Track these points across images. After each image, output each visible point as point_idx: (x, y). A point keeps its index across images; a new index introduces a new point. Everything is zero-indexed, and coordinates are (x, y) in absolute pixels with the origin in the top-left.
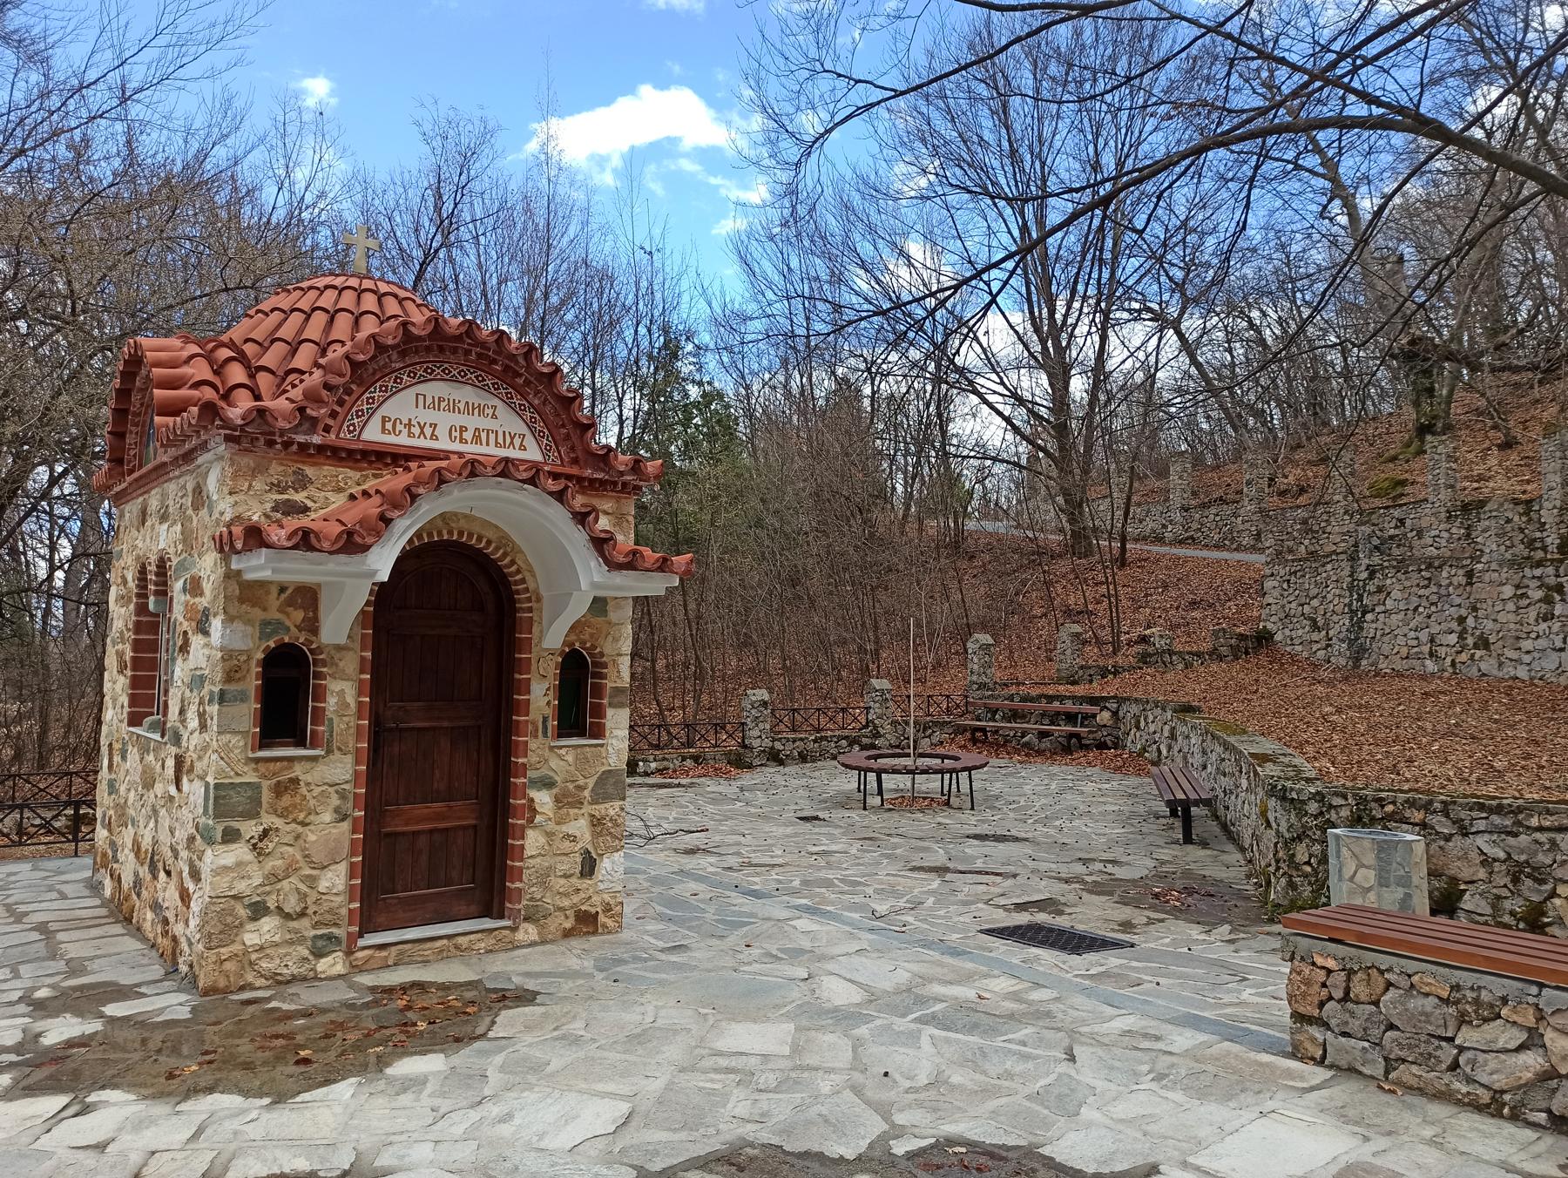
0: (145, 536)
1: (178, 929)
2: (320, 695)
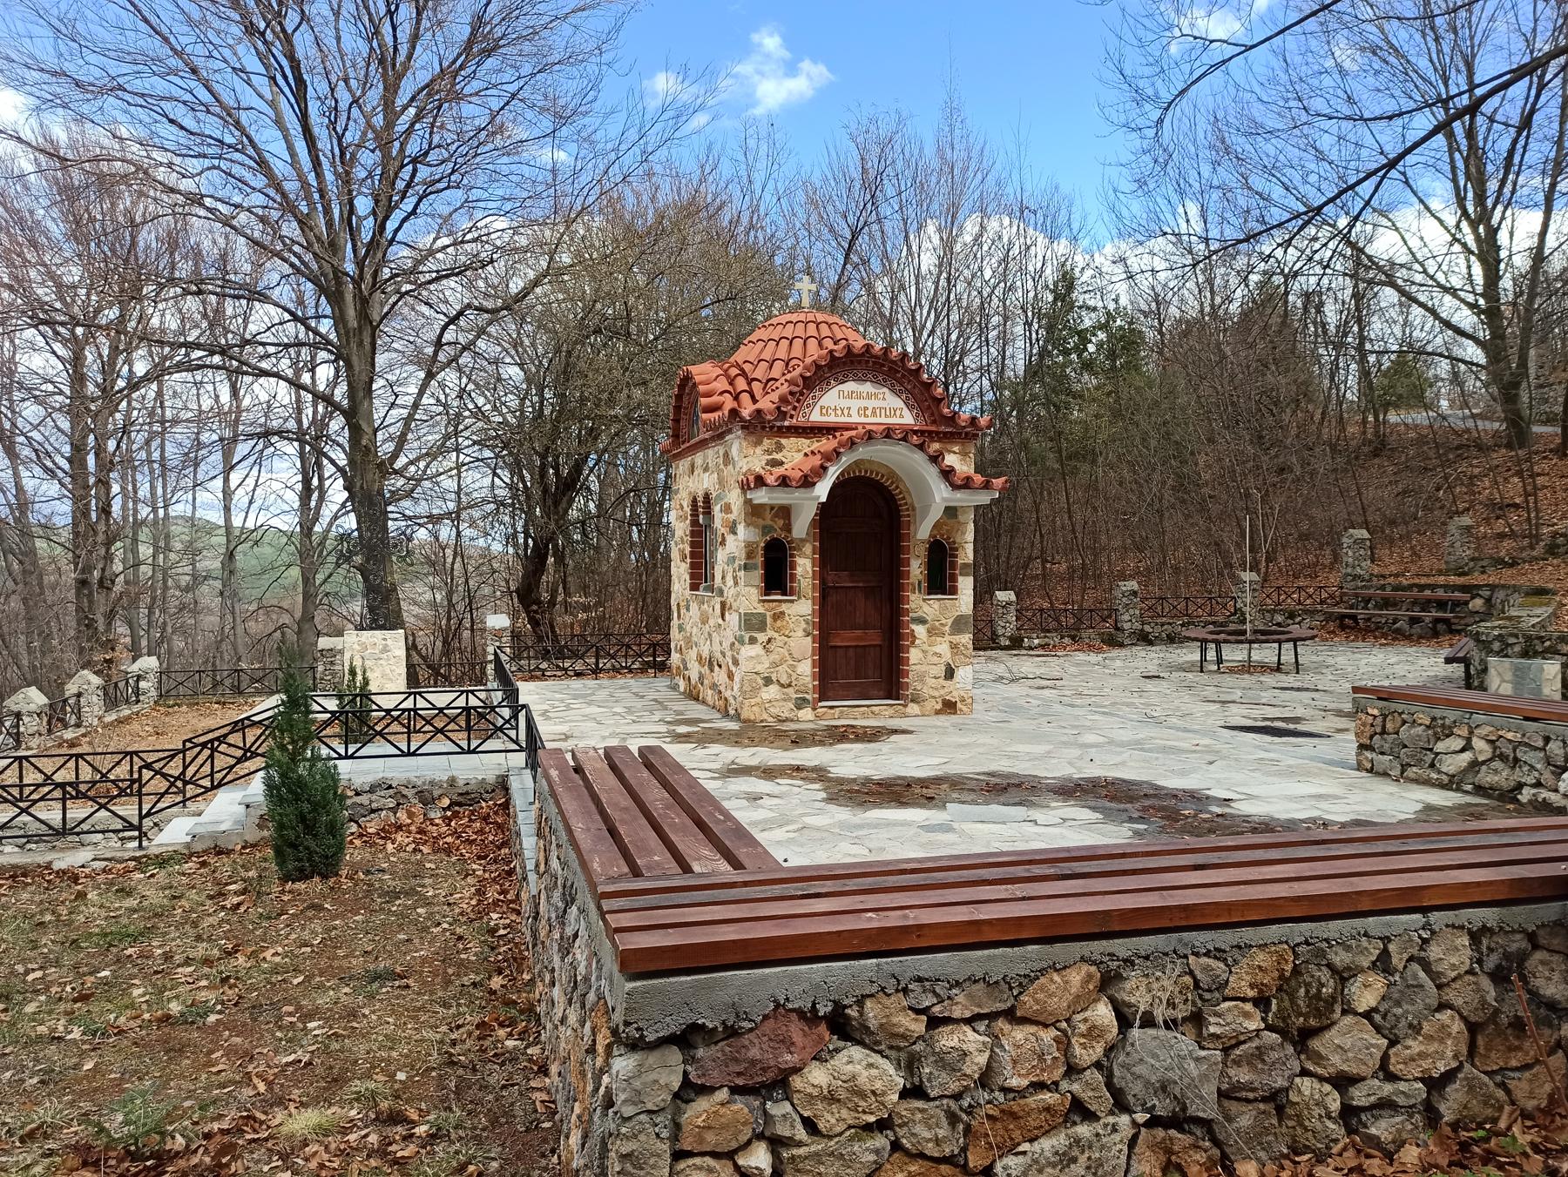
0: (694, 478)
1: (728, 694)
2: (793, 567)
